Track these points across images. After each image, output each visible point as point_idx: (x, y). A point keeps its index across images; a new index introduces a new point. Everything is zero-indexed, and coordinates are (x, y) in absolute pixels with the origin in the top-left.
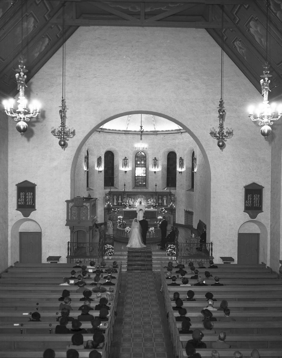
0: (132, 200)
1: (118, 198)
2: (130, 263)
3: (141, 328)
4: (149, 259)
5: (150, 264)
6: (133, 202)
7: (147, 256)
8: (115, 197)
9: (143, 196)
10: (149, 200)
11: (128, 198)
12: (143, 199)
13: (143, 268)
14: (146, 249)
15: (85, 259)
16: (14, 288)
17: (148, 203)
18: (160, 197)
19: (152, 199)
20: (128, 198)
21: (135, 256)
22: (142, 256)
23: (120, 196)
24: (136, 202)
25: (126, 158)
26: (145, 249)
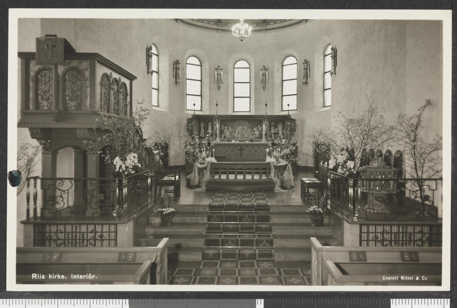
0: (228, 129)
1: (208, 125)
2: (213, 236)
3: (254, 267)
4: (264, 226)
5: (268, 238)
6: (230, 132)
7: (241, 240)
8: (202, 125)
9: (247, 123)
10: (255, 129)
11: (223, 126)
12: (245, 128)
13: (247, 252)
14: (252, 195)
15: (76, 227)
16: (213, 231)
17: (254, 134)
18: (273, 123)
19: (260, 127)
20: (223, 126)
21: (226, 217)
22: (245, 217)
23: (210, 123)
24: (236, 132)
25: (219, 66)
26: (252, 202)
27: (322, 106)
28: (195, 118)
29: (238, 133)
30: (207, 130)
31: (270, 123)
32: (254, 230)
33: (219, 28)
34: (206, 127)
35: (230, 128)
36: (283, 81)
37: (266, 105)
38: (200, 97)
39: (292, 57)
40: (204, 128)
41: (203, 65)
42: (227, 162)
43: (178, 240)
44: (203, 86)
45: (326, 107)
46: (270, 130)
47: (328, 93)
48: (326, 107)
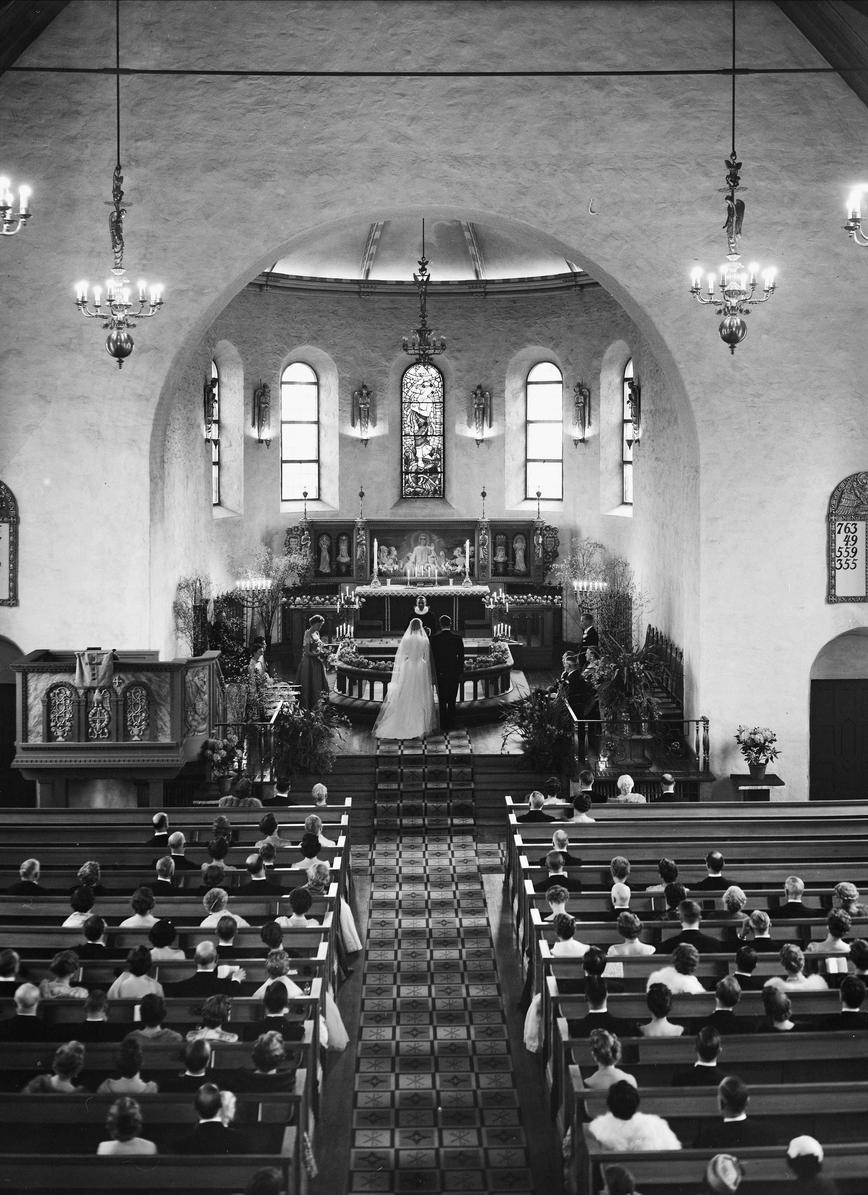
0: (389, 553)
10: (456, 553)
12: (432, 548)
27: (620, 501)
28: (307, 529)
29: (414, 563)
30: (338, 554)
31: (494, 538)
32: (453, 829)
33: (363, 290)
34: (334, 549)
35: (393, 549)
36: (527, 422)
37: (484, 494)
38: (315, 387)
39: (540, 366)
40: (330, 551)
41: (322, 382)
42: (209, 802)
43: (258, 897)
44: (322, 434)
45: (626, 504)
46: (495, 555)
47: (628, 469)
48: (626, 504)
